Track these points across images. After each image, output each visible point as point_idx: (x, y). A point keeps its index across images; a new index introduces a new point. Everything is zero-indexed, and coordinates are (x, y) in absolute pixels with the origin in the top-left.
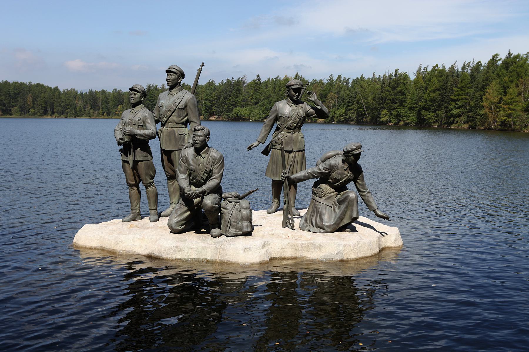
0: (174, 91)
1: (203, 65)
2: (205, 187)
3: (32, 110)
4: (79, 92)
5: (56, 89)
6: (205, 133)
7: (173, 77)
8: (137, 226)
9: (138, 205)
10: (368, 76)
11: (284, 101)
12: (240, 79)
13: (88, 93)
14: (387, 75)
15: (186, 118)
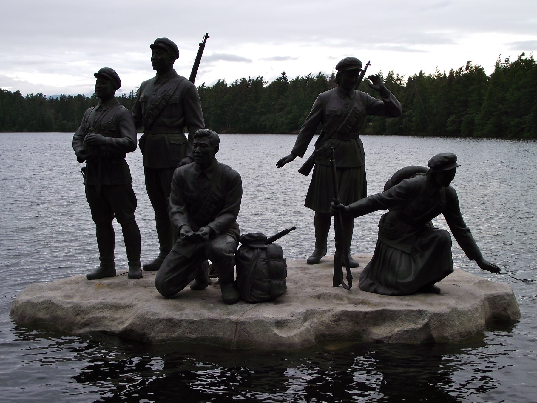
1: (207, 36)
4: (47, 97)
5: (18, 93)
12: (259, 79)
13: (59, 99)
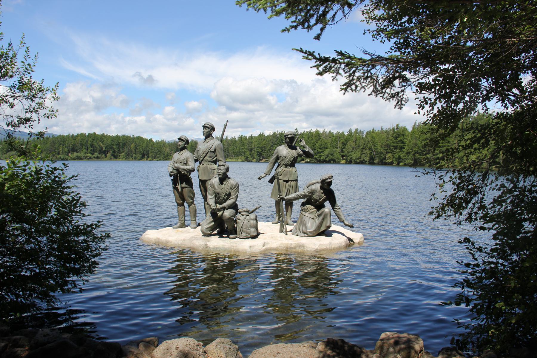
0: (208, 140)
1: (228, 122)
2: (225, 205)
3: (134, 155)
6: (225, 167)
7: (207, 130)
8: (181, 232)
9: (184, 217)
10: (378, 129)
11: (283, 146)
14: (391, 128)
15: (216, 158)
